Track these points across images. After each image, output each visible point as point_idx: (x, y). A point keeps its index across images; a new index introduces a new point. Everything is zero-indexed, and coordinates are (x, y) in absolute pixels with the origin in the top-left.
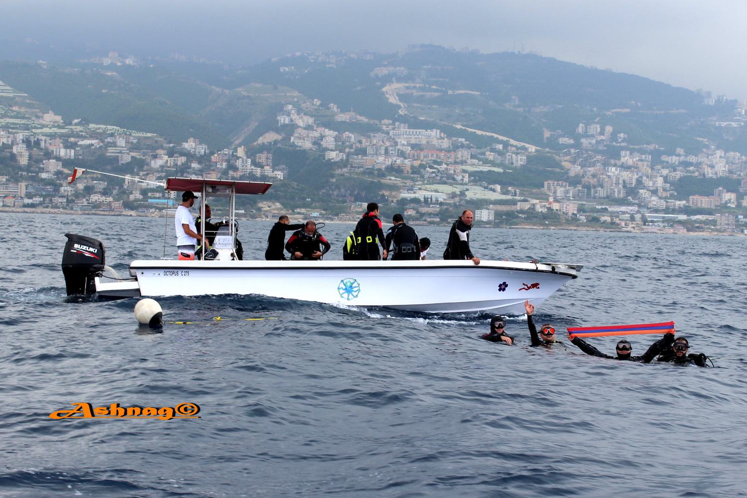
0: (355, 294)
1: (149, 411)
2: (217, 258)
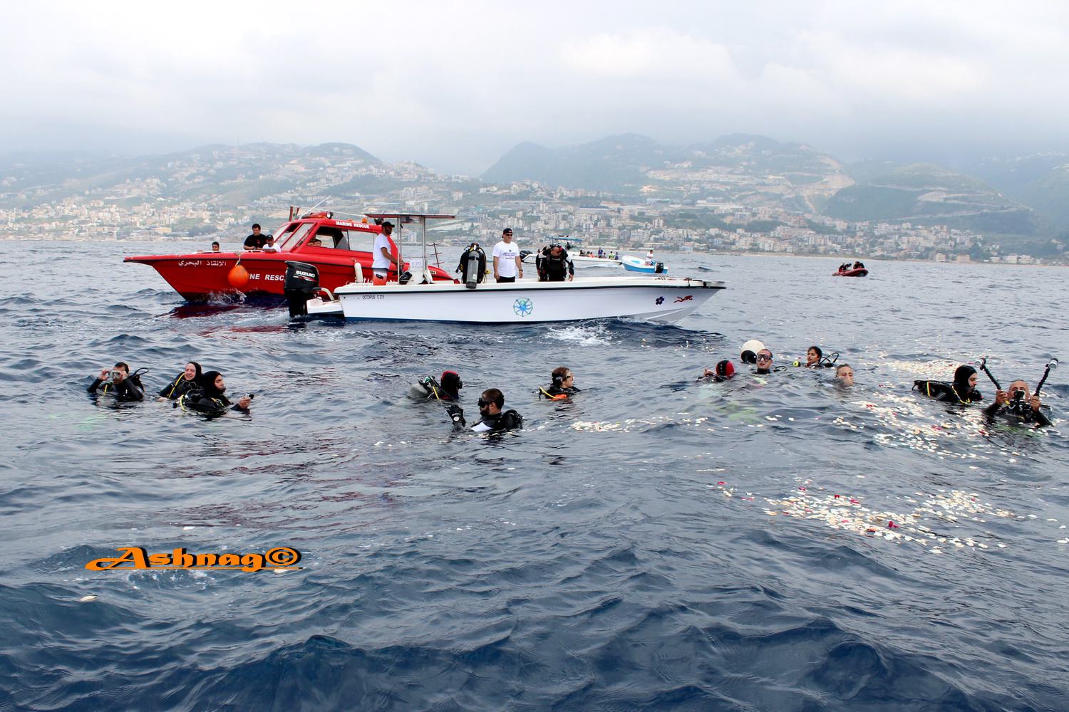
0: (528, 311)
1: (228, 559)
2: (411, 279)
